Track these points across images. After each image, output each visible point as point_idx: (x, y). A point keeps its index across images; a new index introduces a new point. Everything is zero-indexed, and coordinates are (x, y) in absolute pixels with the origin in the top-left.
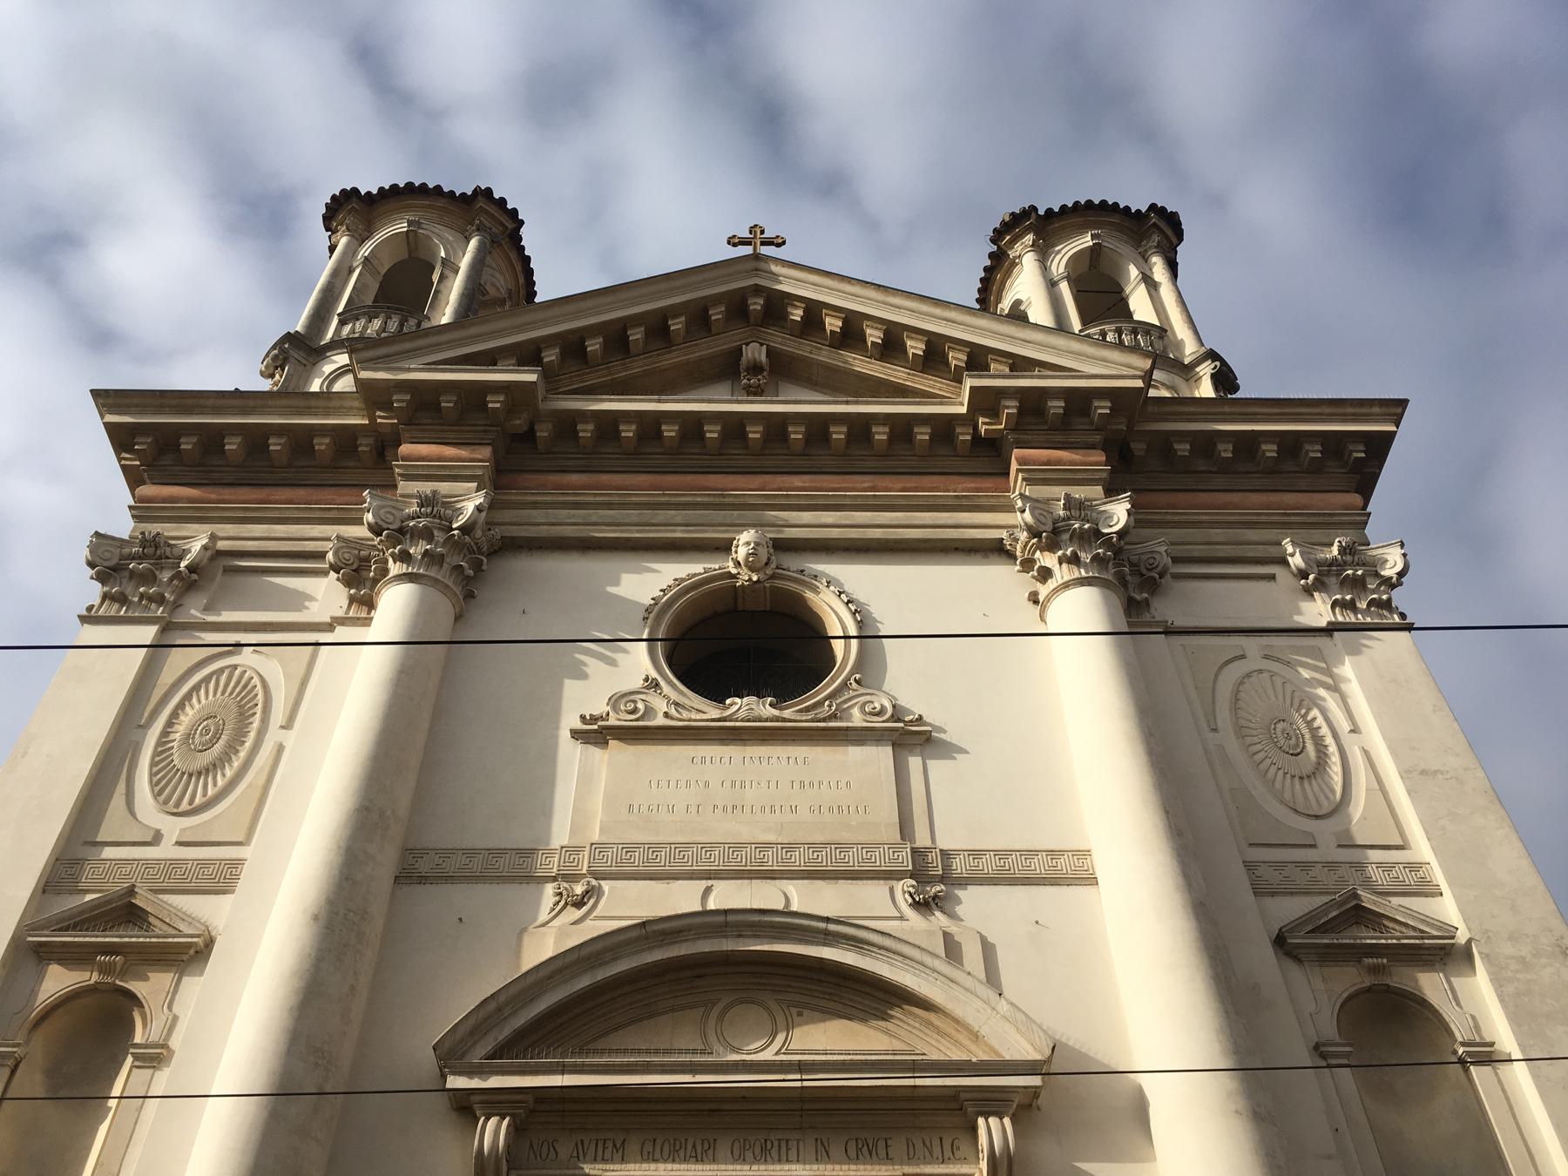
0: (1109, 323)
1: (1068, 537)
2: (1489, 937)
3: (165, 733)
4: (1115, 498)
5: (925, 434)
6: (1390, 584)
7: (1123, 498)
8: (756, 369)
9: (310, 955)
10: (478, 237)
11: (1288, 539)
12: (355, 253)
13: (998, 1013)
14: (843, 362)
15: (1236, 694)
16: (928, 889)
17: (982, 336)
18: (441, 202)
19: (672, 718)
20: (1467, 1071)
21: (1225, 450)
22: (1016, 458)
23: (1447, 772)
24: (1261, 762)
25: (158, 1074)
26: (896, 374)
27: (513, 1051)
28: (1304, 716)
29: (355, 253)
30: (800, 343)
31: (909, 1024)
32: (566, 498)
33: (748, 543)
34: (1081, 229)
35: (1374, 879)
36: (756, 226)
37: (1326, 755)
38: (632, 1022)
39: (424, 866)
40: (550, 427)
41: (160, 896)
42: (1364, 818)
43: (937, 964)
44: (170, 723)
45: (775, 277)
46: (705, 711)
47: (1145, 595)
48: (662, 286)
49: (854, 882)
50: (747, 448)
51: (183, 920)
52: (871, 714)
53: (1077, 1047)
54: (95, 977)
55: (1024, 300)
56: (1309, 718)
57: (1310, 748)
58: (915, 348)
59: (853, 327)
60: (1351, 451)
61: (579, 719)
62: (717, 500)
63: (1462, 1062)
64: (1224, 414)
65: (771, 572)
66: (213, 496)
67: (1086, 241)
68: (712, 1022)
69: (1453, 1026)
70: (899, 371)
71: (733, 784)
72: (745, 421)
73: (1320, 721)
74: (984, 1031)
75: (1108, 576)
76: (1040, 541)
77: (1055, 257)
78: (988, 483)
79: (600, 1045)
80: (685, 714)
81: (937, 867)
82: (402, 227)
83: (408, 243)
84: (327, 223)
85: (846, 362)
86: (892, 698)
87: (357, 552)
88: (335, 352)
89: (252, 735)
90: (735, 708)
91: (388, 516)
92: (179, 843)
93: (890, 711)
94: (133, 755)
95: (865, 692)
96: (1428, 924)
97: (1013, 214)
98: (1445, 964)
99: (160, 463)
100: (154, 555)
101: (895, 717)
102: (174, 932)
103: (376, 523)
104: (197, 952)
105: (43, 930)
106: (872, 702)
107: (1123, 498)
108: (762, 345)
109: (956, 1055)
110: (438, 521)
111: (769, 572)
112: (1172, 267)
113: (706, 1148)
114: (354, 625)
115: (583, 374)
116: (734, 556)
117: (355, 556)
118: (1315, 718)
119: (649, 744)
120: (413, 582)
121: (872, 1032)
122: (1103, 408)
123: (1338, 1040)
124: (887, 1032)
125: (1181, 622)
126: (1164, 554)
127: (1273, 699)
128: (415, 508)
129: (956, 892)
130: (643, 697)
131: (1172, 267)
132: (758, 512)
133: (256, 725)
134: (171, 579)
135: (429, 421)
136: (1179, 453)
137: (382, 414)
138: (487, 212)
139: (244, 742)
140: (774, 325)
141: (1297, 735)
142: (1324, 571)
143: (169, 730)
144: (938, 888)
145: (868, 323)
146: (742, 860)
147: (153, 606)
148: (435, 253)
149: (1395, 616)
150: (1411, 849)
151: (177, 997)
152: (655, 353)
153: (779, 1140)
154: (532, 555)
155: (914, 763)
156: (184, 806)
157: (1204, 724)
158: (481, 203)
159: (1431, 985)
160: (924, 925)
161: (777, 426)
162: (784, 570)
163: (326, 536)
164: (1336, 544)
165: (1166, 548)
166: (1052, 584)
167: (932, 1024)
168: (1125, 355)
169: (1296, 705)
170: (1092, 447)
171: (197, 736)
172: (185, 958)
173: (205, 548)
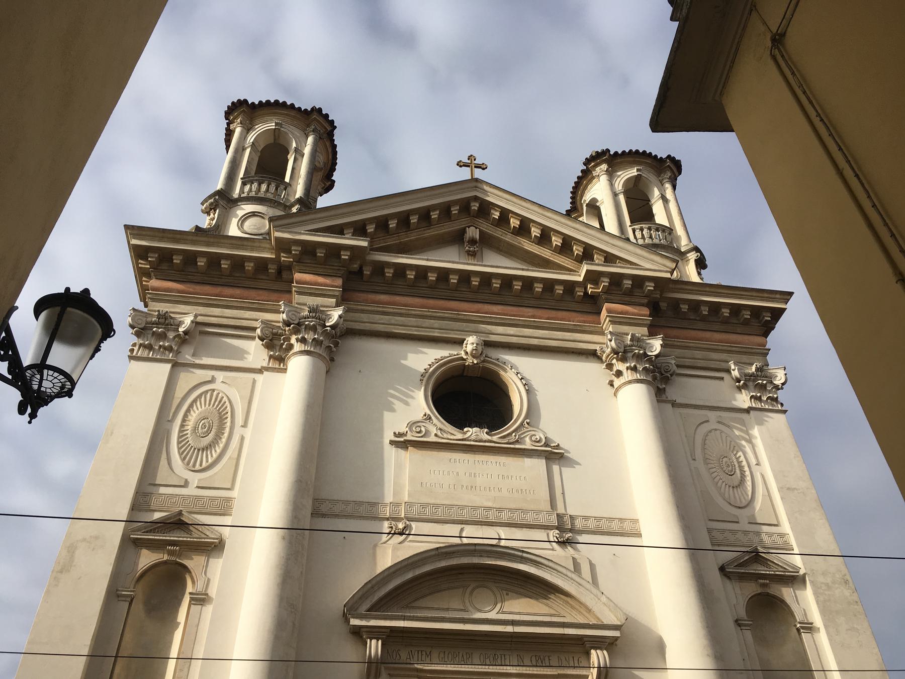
0: (645, 224)
1: (632, 355)
2: (814, 573)
3: (182, 426)
5: (560, 290)
6: (777, 388)
8: (473, 242)
9: (283, 557)
10: (313, 136)
11: (732, 362)
13: (601, 601)
14: (518, 243)
15: (705, 441)
17: (591, 239)
18: (293, 113)
20: (800, 633)
21: (705, 311)
22: (606, 307)
23: (799, 489)
25: (204, 608)
26: (545, 253)
27: (380, 607)
28: (735, 455)
29: (245, 138)
30: (496, 230)
31: (558, 602)
33: (473, 344)
34: (632, 164)
36: (471, 155)
38: (430, 594)
39: (324, 509)
40: (371, 269)
41: (193, 515)
42: (760, 509)
43: (569, 574)
45: (485, 192)
46: (454, 435)
47: (664, 386)
48: (429, 193)
49: (531, 530)
50: (470, 288)
51: (209, 530)
52: (535, 441)
53: (633, 617)
54: (166, 557)
55: (599, 200)
56: (737, 456)
58: (557, 241)
59: (524, 228)
60: (764, 316)
61: (393, 433)
63: (798, 630)
64: (705, 291)
65: (483, 359)
66: (191, 290)
67: (633, 172)
68: (467, 595)
69: (795, 614)
70: (547, 252)
71: (470, 475)
72: (471, 275)
73: (742, 458)
76: (618, 356)
77: (616, 180)
78: (590, 318)
79: (416, 604)
80: (445, 436)
82: (272, 126)
83: (275, 135)
84: (227, 116)
86: (544, 433)
87: (271, 330)
88: (243, 203)
89: (227, 430)
90: (469, 434)
91: (293, 316)
92: (198, 487)
94: (167, 437)
95: (532, 429)
96: (788, 565)
97: (597, 152)
98: (793, 584)
99: (160, 268)
100: (164, 323)
101: (546, 445)
102: (206, 536)
103: (288, 320)
104: (215, 546)
105: (138, 532)
106: (535, 435)
108: (476, 228)
109: (582, 621)
111: (482, 359)
113: (468, 657)
114: (273, 371)
116: (464, 348)
118: (740, 456)
119: (428, 450)
120: (308, 355)
121: (540, 604)
122: (650, 286)
123: (746, 618)
124: (547, 605)
128: (306, 313)
129: (577, 537)
130: (424, 424)
132: (476, 325)
133: (228, 424)
134: (174, 337)
136: (683, 310)
137: (284, 255)
139: (223, 433)
140: (482, 218)
141: (732, 465)
143: (184, 424)
144: (569, 535)
145: (534, 224)
146: (479, 515)
147: (167, 352)
148: (290, 144)
149: (779, 405)
150: (781, 526)
151: (208, 569)
152: (423, 229)
154: (361, 338)
155: (556, 468)
156: (197, 467)
158: (315, 116)
159: (787, 593)
161: (486, 278)
162: (489, 358)
163: (258, 318)
166: (622, 380)
167: (568, 602)
168: (663, 259)
169: (732, 449)
170: (643, 305)
171: (200, 428)
172: (209, 549)
173: (192, 322)
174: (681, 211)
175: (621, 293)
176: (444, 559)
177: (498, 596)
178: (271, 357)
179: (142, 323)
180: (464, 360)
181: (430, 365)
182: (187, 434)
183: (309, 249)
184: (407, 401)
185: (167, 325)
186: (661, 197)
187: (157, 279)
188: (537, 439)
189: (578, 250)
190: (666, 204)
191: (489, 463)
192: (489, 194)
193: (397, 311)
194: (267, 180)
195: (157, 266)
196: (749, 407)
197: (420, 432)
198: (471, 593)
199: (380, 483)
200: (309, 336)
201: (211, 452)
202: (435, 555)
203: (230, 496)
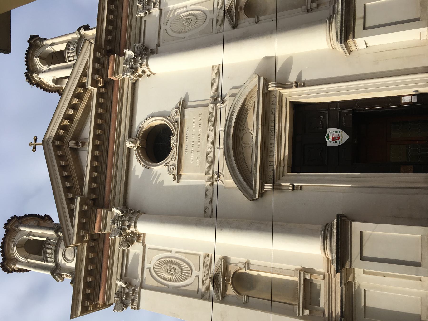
0: (66, 55)
3: (171, 281)
4: (125, 53)
7: (125, 51)
8: (77, 144)
9: (230, 230)
12: (22, 262)
13: (248, 85)
14: (77, 121)
16: (219, 101)
18: (7, 238)
19: (175, 159)
21: (111, 27)
24: (193, 28)
25: (251, 264)
26: (82, 107)
27: (251, 185)
28: (182, 18)
29: (22, 262)
32: (113, 190)
33: (130, 143)
34: (33, 61)
35: (221, 7)
36: (29, 144)
37: (191, 14)
39: (208, 212)
41: (212, 272)
42: (207, 7)
43: (237, 99)
44: (168, 280)
45: (50, 137)
46: (174, 152)
47: (149, 50)
48: (51, 167)
49: (217, 116)
52: (177, 114)
53: (255, 70)
54: (230, 283)
55: (53, 78)
57: (190, 17)
59: (70, 118)
61: (174, 181)
62: (116, 152)
64: (101, 26)
67: (37, 60)
70: (82, 106)
72: (94, 145)
73: (183, 14)
74: (251, 88)
75: (146, 57)
77: (41, 69)
78: (116, 85)
79: (250, 168)
80: (175, 156)
81: (215, 99)
82: (15, 249)
85: (77, 120)
86: (173, 109)
87: (124, 242)
88: (58, 261)
90: (174, 145)
91: (117, 232)
93: (177, 109)
101: (178, 108)
102: (221, 265)
103: (119, 234)
105: (219, 296)
106: (174, 113)
107: (125, 51)
108: (69, 142)
109: (256, 94)
110: (119, 219)
111: (137, 139)
112: (45, 39)
115: (76, 187)
116: (132, 148)
117: (125, 243)
120: (136, 223)
122: (99, 54)
123: (255, 18)
124: (250, 109)
125: (156, 43)
126: (139, 44)
127: (177, 24)
128: (115, 226)
130: (169, 167)
131: (45, 39)
133: (170, 259)
134: (128, 289)
135: (88, 226)
136: (111, 38)
137: (85, 238)
138: (12, 225)
139: (174, 261)
140: (64, 139)
142: (145, 9)
143: (170, 280)
144: (220, 98)
145: (67, 113)
146: (211, 140)
147: (135, 292)
148: (25, 239)
153: (271, 130)
155: (189, 104)
157: (182, 40)
158: (9, 227)
160: (228, 101)
161: (96, 137)
164: (138, 5)
165: (137, 44)
166: (147, 70)
167: (249, 100)
169: (179, 19)
172: (226, 263)
173: (120, 281)
174: (58, 37)
175: (103, 69)
176: (231, 156)
177: (246, 132)
178: (137, 241)
179: (121, 305)
180: (137, 148)
181: (141, 164)
182: (175, 278)
183: (82, 226)
184: (158, 175)
185: (122, 293)
186: (51, 46)
187: (98, 300)
188: (176, 113)
189: (80, 90)
190: (54, 44)
191: (187, 135)
192: (50, 136)
193: (114, 181)
194: (45, 249)
195: (92, 300)
196: (159, 9)
197: (173, 169)
198: (245, 144)
199: (196, 187)
200: (127, 223)
201: (183, 266)
202: (229, 161)
203: (203, 256)
